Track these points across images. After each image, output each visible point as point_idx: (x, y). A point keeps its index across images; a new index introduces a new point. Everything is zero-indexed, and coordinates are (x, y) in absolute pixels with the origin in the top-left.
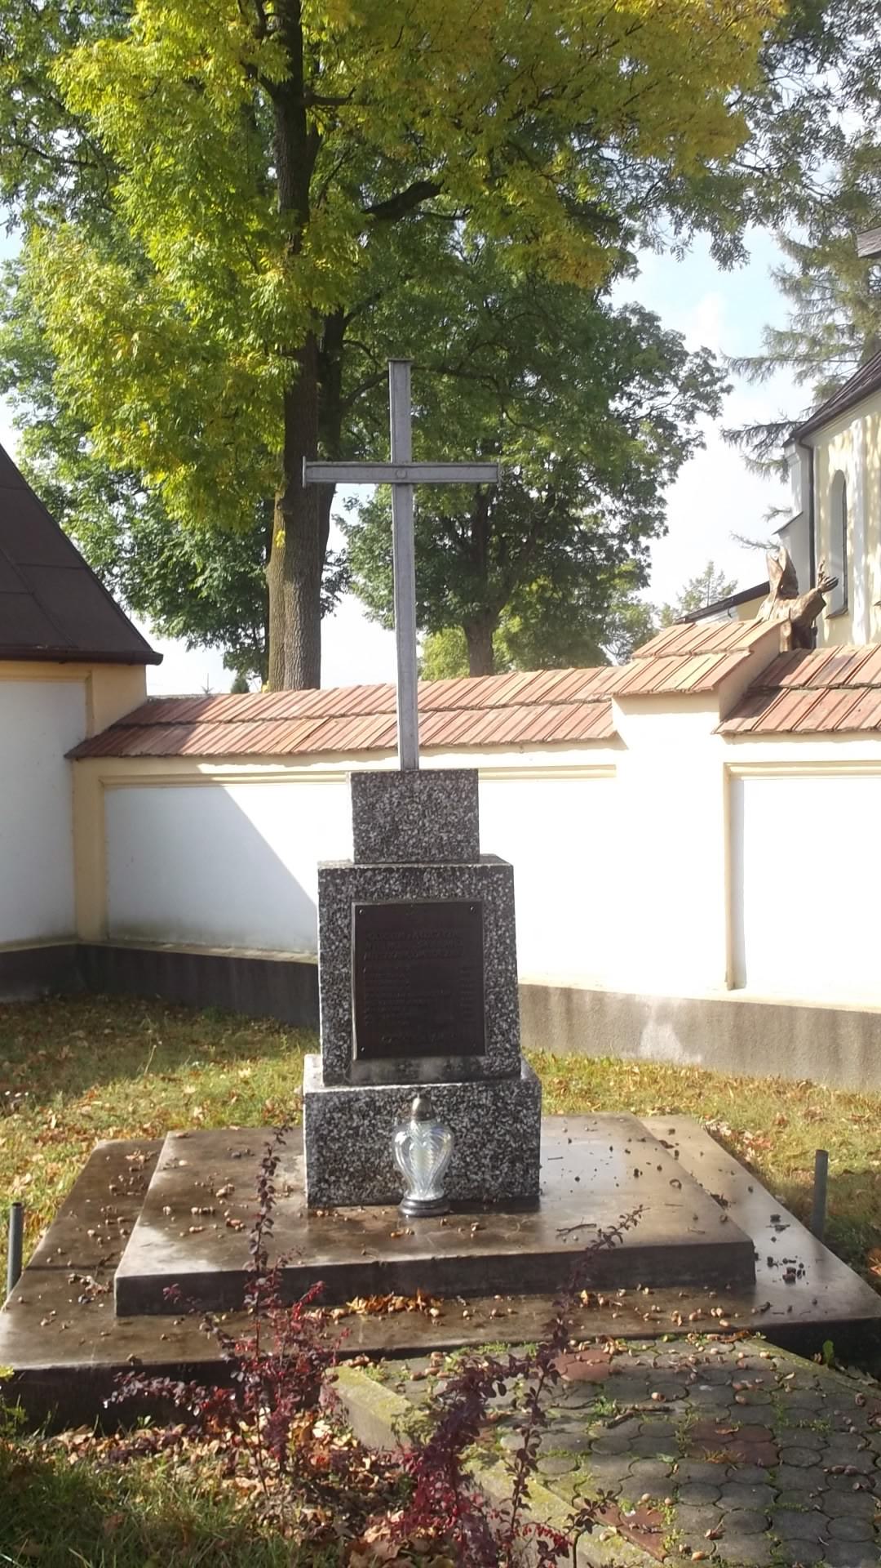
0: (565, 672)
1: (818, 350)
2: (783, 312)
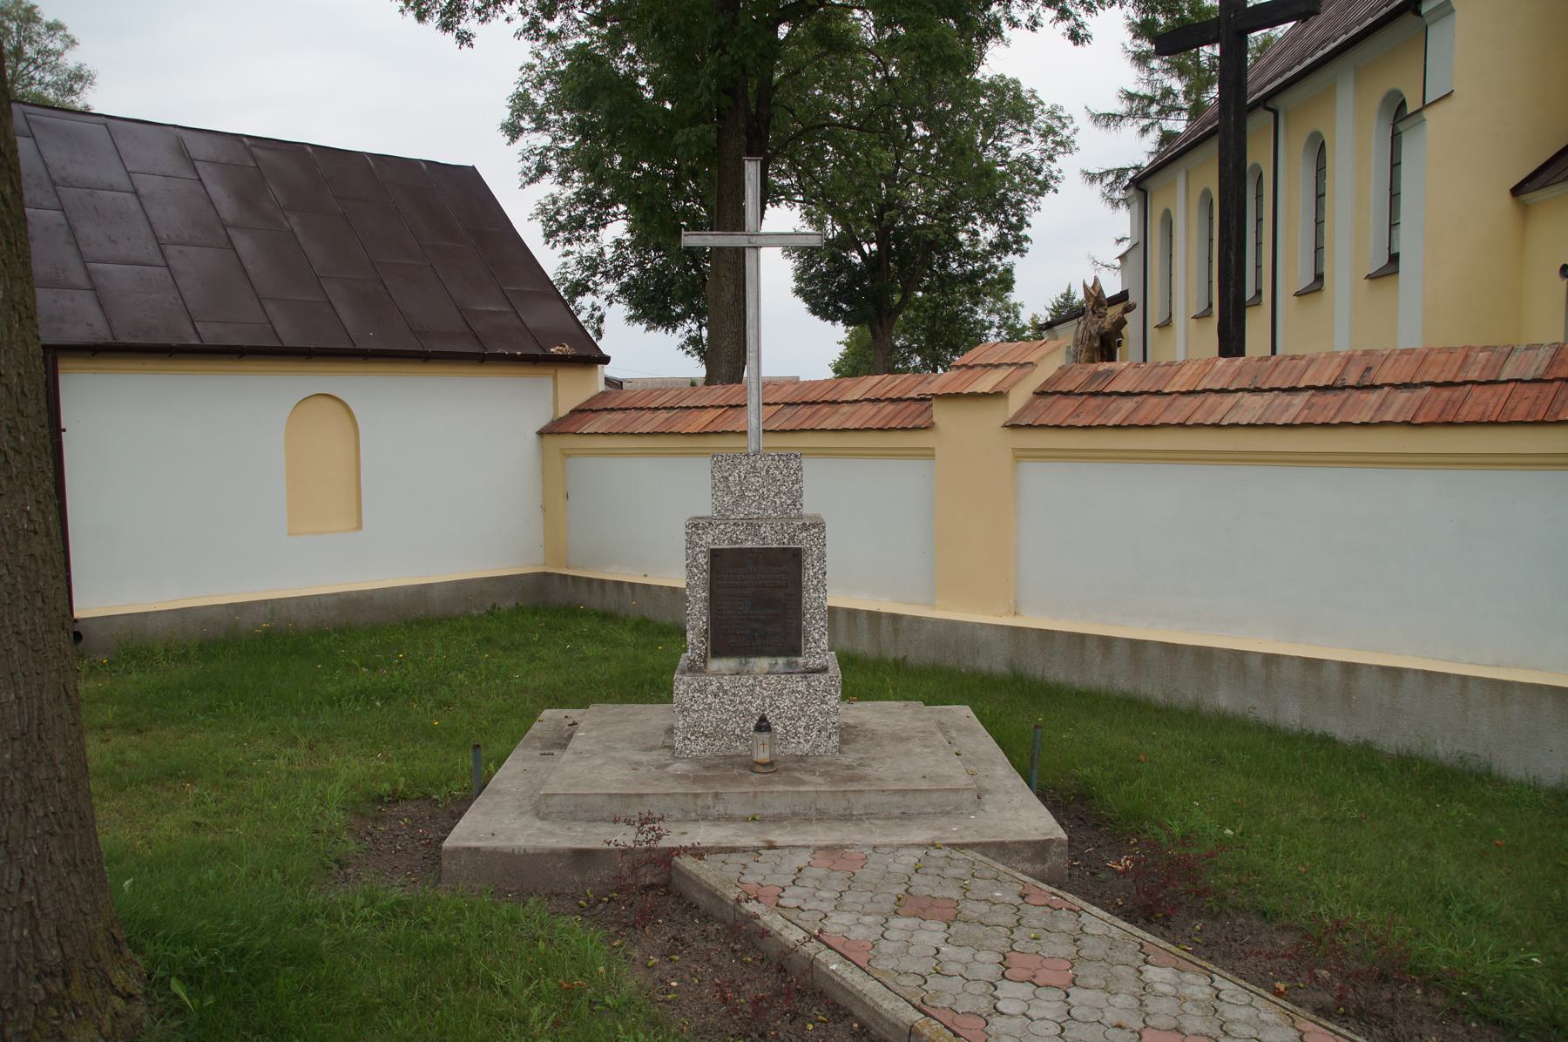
0: (877, 378)
1: (1163, 102)
2: (1133, 79)
